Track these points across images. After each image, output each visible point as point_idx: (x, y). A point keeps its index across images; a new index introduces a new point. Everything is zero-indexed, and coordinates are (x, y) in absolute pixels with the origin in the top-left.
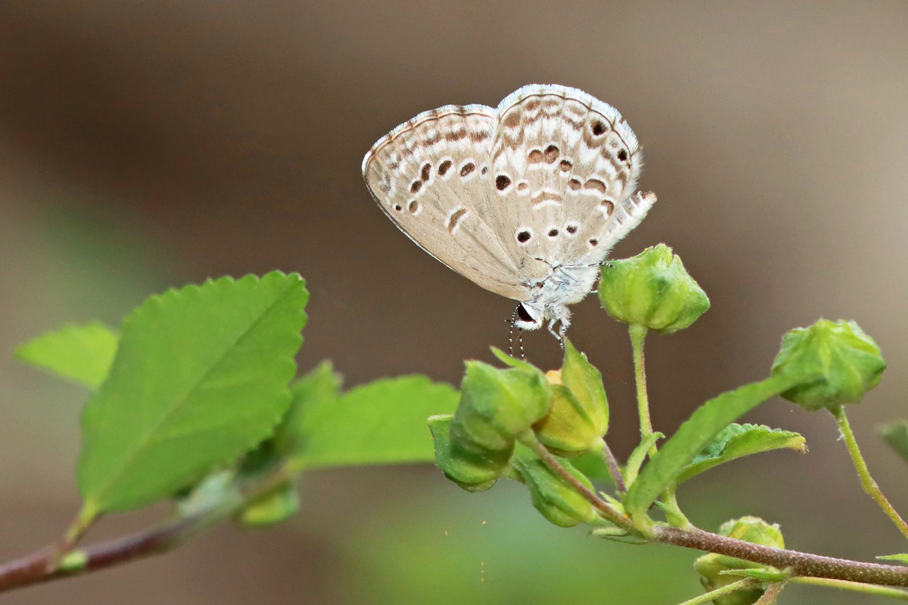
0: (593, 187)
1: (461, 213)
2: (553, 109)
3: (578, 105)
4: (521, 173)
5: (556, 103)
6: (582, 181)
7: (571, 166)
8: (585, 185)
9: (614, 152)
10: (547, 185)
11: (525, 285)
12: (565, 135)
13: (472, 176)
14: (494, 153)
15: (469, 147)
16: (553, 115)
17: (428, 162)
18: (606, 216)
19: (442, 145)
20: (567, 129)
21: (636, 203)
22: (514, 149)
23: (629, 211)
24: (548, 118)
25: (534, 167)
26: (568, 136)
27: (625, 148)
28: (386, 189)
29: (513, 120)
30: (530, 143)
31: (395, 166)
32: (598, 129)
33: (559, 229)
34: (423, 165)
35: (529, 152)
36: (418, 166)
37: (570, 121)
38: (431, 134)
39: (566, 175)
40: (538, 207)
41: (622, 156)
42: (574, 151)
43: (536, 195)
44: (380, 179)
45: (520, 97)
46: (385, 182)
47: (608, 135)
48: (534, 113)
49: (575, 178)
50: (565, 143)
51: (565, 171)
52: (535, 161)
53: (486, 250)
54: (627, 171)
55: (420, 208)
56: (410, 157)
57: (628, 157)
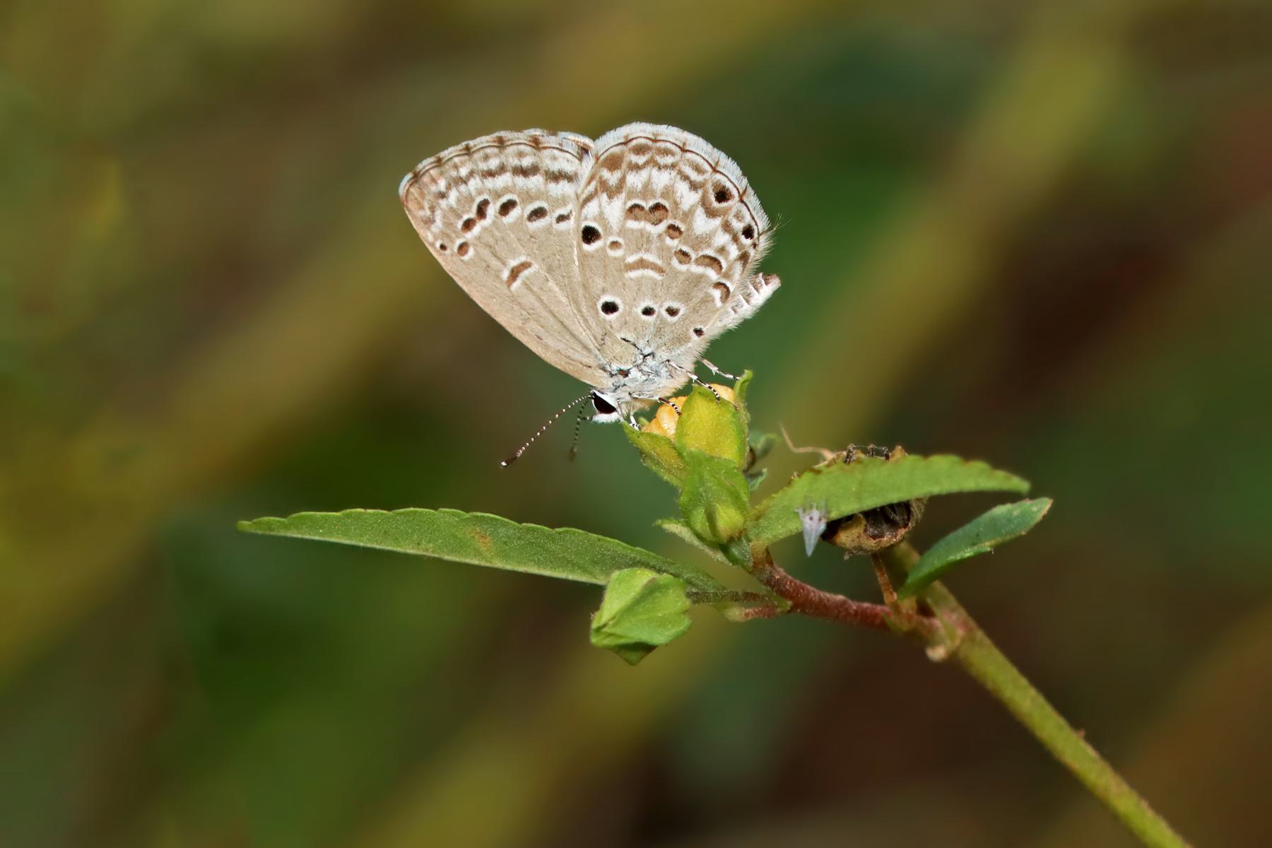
0: (707, 265)
1: (525, 266)
2: (669, 160)
3: (701, 161)
4: (615, 228)
5: (673, 154)
6: (693, 256)
7: (681, 233)
8: (697, 260)
9: (738, 226)
10: (647, 250)
11: (604, 369)
12: (679, 194)
13: (540, 223)
14: (584, 196)
15: (542, 187)
16: (666, 167)
17: (486, 197)
18: (718, 303)
19: (504, 180)
20: (682, 187)
21: (757, 290)
22: (610, 197)
23: (748, 298)
24: (465, 183)
25: (632, 224)
26: (682, 197)
27: (753, 224)
28: (429, 222)
29: (613, 163)
30: (631, 194)
31: (443, 195)
32: (722, 195)
33: (655, 307)
34: (479, 200)
35: (630, 204)
36: (473, 200)
37: (686, 178)
38: (493, 164)
39: (674, 244)
40: (634, 274)
41: (748, 232)
42: (688, 216)
43: (631, 259)
44: (422, 208)
45: (626, 137)
46: (428, 213)
47: (733, 204)
48: (641, 160)
49: (685, 249)
50: (676, 204)
51: (672, 238)
52: (636, 219)
53: (554, 316)
54: (752, 252)
55: (471, 252)
56: (463, 188)
57: (756, 235)
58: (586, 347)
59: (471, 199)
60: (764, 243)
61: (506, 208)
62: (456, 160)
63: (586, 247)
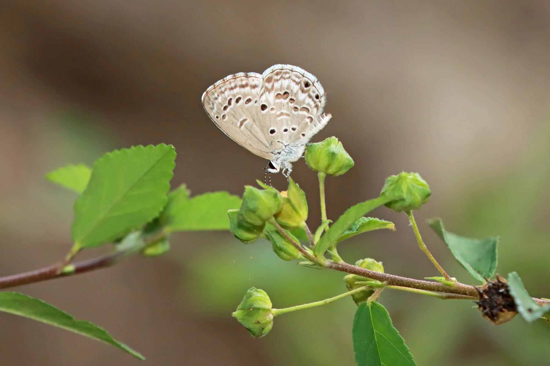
1: (245, 120)
2: (287, 76)
3: (298, 74)
4: (272, 103)
5: (288, 73)
9: (314, 95)
11: (272, 153)
13: (250, 104)
16: (287, 78)
17: (231, 97)
18: (309, 123)
19: (237, 90)
20: (293, 85)
22: (269, 93)
23: (320, 121)
25: (278, 101)
28: (212, 109)
29: (269, 80)
30: (276, 90)
32: (307, 85)
33: (288, 128)
34: (229, 98)
37: (294, 81)
38: (233, 85)
39: (292, 105)
40: (279, 118)
41: (317, 97)
42: (296, 94)
43: (278, 113)
44: (209, 104)
46: (212, 106)
47: (311, 88)
48: (278, 77)
49: (296, 106)
50: (292, 91)
52: (279, 98)
53: (256, 137)
54: (319, 104)
55: (227, 118)
56: (223, 95)
58: (266, 147)
59: (225, 99)
60: (323, 100)
61: (237, 101)
62: (231, 80)
63: (262, 112)
